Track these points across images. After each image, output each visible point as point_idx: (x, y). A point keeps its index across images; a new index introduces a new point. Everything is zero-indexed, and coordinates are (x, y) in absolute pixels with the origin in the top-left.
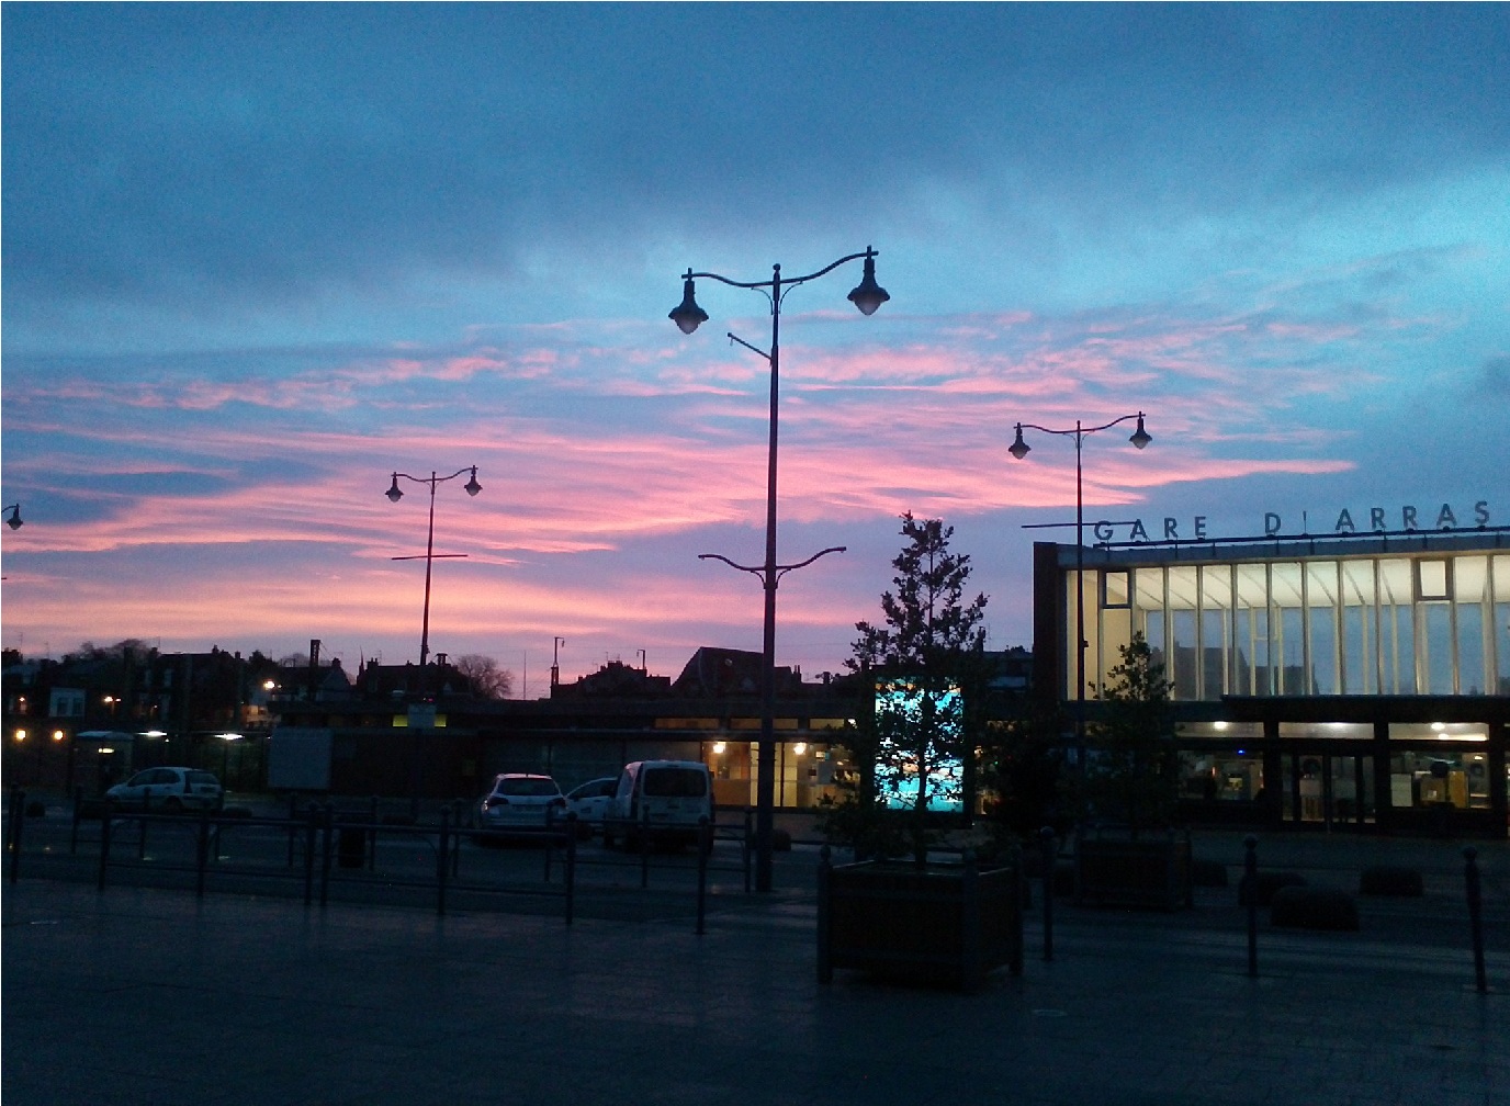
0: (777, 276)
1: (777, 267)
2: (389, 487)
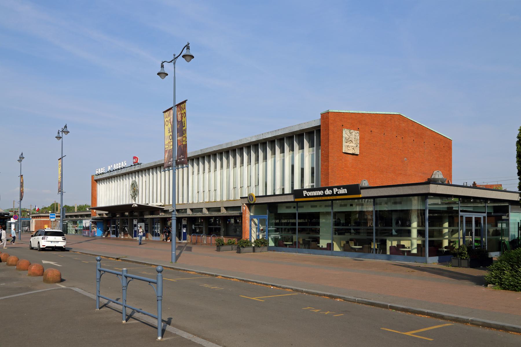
2: (57, 135)
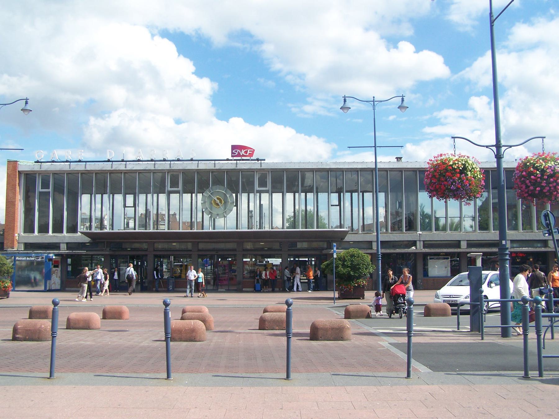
0: (374, 99)
1: (374, 97)
2: (342, 104)
